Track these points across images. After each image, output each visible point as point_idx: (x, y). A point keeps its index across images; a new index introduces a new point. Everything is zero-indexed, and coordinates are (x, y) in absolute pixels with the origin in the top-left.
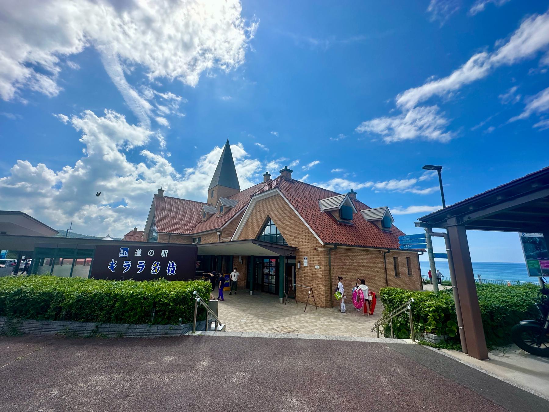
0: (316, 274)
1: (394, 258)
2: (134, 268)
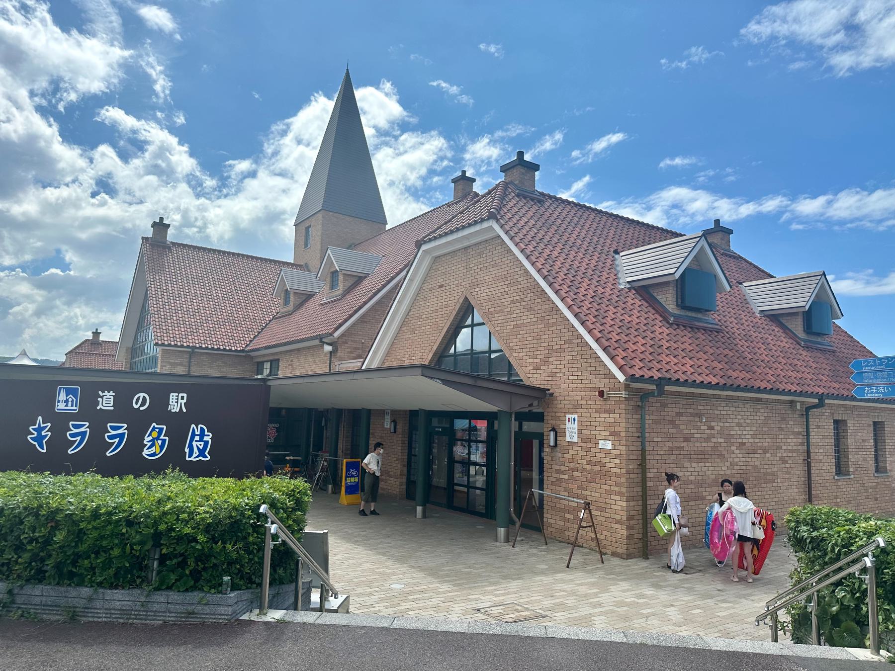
0: (602, 465)
1: (875, 423)
2: (97, 442)
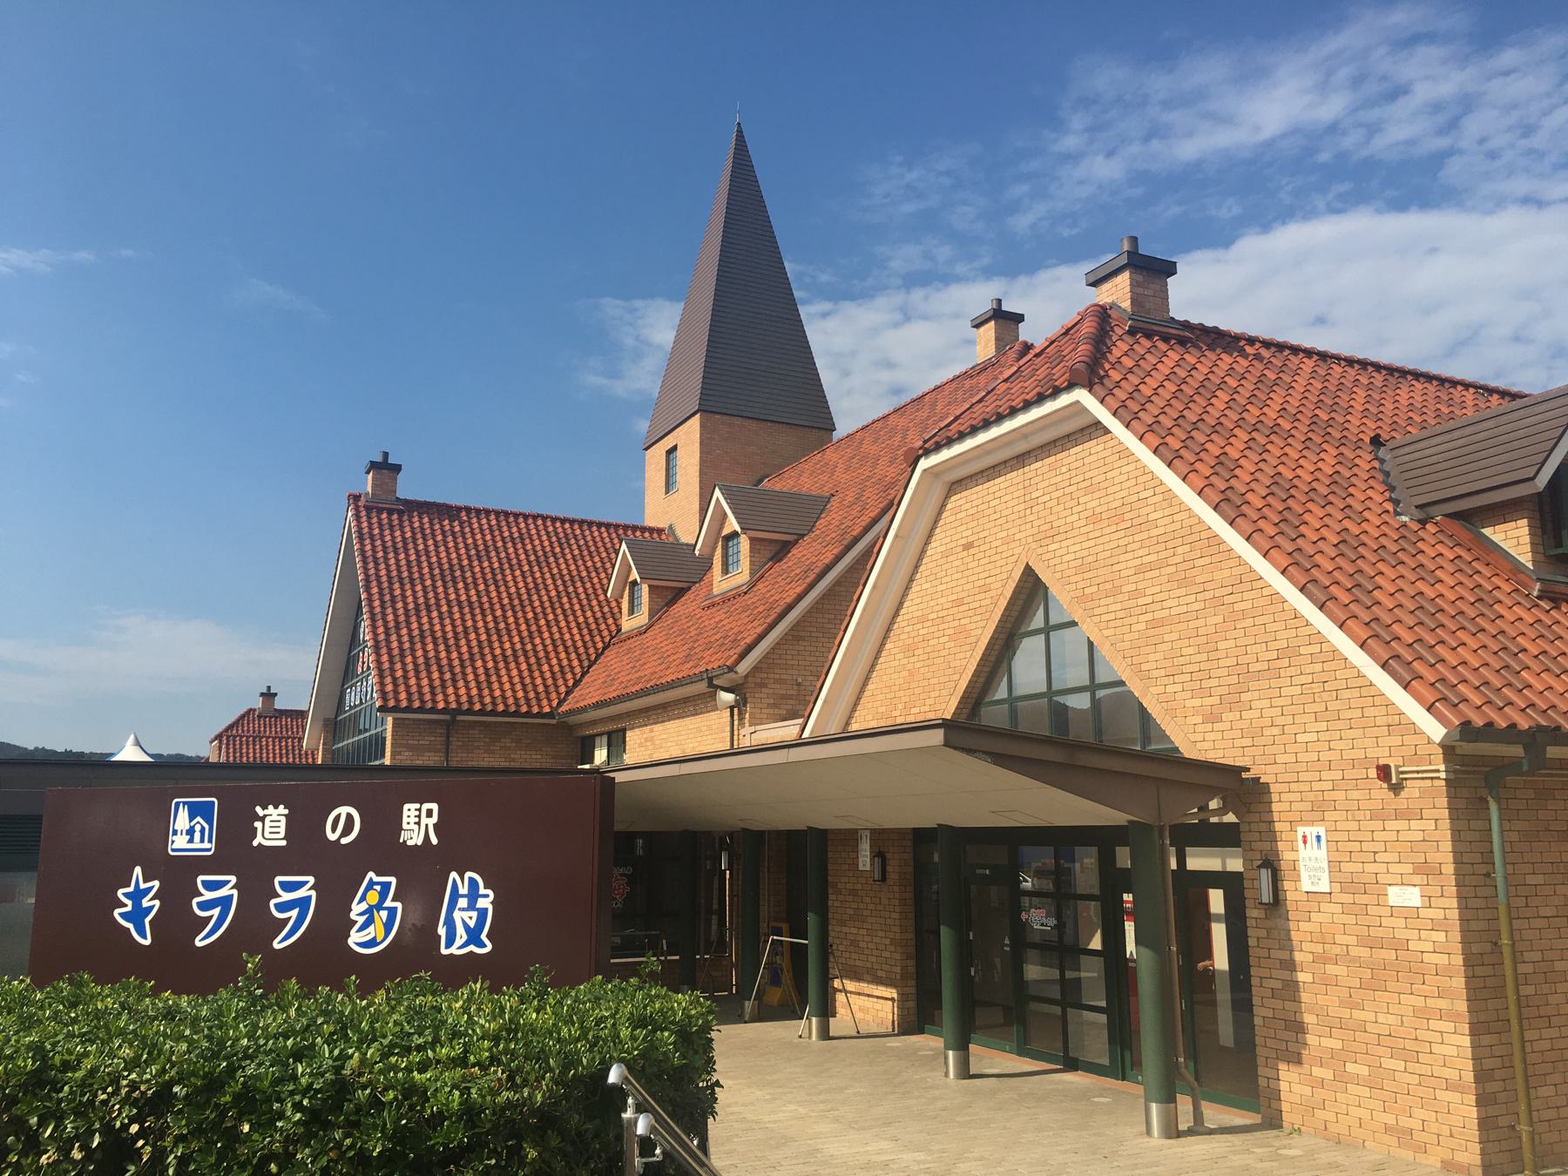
0: (1401, 946)
2: (253, 922)
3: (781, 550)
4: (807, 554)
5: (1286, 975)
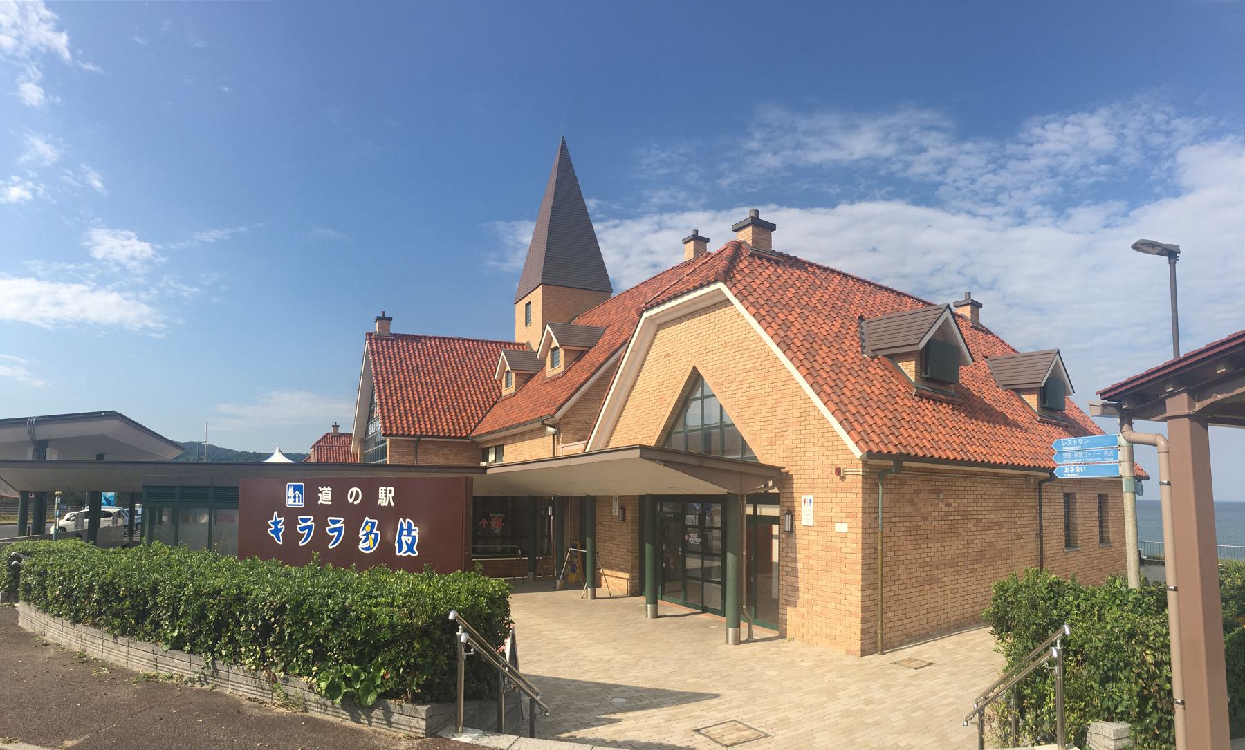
1: (1100, 495)
3: (581, 355)
4: (593, 357)
5: (792, 565)
